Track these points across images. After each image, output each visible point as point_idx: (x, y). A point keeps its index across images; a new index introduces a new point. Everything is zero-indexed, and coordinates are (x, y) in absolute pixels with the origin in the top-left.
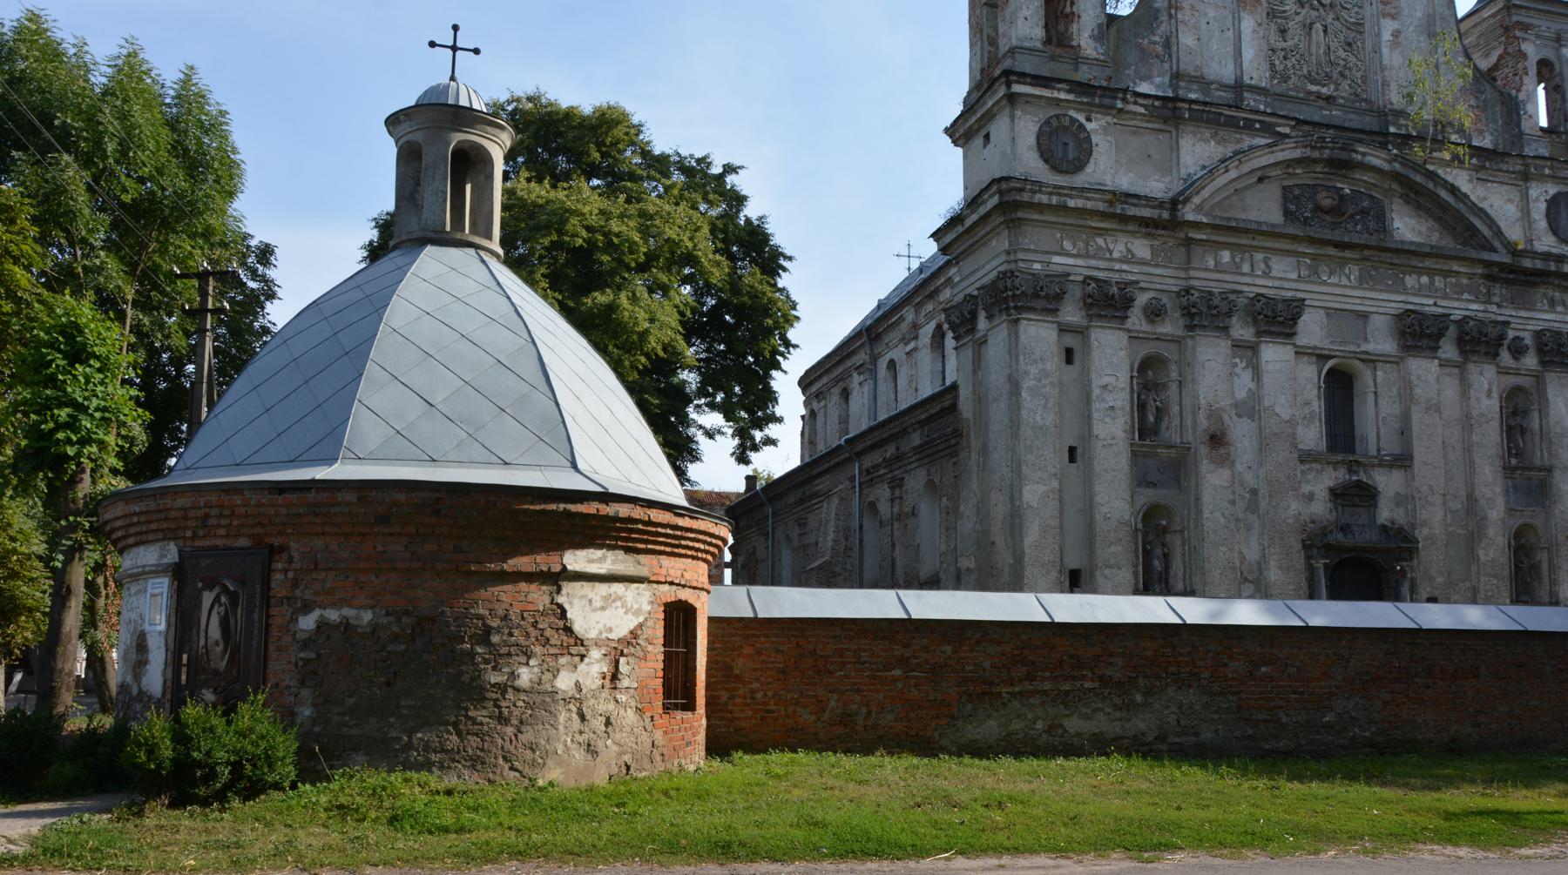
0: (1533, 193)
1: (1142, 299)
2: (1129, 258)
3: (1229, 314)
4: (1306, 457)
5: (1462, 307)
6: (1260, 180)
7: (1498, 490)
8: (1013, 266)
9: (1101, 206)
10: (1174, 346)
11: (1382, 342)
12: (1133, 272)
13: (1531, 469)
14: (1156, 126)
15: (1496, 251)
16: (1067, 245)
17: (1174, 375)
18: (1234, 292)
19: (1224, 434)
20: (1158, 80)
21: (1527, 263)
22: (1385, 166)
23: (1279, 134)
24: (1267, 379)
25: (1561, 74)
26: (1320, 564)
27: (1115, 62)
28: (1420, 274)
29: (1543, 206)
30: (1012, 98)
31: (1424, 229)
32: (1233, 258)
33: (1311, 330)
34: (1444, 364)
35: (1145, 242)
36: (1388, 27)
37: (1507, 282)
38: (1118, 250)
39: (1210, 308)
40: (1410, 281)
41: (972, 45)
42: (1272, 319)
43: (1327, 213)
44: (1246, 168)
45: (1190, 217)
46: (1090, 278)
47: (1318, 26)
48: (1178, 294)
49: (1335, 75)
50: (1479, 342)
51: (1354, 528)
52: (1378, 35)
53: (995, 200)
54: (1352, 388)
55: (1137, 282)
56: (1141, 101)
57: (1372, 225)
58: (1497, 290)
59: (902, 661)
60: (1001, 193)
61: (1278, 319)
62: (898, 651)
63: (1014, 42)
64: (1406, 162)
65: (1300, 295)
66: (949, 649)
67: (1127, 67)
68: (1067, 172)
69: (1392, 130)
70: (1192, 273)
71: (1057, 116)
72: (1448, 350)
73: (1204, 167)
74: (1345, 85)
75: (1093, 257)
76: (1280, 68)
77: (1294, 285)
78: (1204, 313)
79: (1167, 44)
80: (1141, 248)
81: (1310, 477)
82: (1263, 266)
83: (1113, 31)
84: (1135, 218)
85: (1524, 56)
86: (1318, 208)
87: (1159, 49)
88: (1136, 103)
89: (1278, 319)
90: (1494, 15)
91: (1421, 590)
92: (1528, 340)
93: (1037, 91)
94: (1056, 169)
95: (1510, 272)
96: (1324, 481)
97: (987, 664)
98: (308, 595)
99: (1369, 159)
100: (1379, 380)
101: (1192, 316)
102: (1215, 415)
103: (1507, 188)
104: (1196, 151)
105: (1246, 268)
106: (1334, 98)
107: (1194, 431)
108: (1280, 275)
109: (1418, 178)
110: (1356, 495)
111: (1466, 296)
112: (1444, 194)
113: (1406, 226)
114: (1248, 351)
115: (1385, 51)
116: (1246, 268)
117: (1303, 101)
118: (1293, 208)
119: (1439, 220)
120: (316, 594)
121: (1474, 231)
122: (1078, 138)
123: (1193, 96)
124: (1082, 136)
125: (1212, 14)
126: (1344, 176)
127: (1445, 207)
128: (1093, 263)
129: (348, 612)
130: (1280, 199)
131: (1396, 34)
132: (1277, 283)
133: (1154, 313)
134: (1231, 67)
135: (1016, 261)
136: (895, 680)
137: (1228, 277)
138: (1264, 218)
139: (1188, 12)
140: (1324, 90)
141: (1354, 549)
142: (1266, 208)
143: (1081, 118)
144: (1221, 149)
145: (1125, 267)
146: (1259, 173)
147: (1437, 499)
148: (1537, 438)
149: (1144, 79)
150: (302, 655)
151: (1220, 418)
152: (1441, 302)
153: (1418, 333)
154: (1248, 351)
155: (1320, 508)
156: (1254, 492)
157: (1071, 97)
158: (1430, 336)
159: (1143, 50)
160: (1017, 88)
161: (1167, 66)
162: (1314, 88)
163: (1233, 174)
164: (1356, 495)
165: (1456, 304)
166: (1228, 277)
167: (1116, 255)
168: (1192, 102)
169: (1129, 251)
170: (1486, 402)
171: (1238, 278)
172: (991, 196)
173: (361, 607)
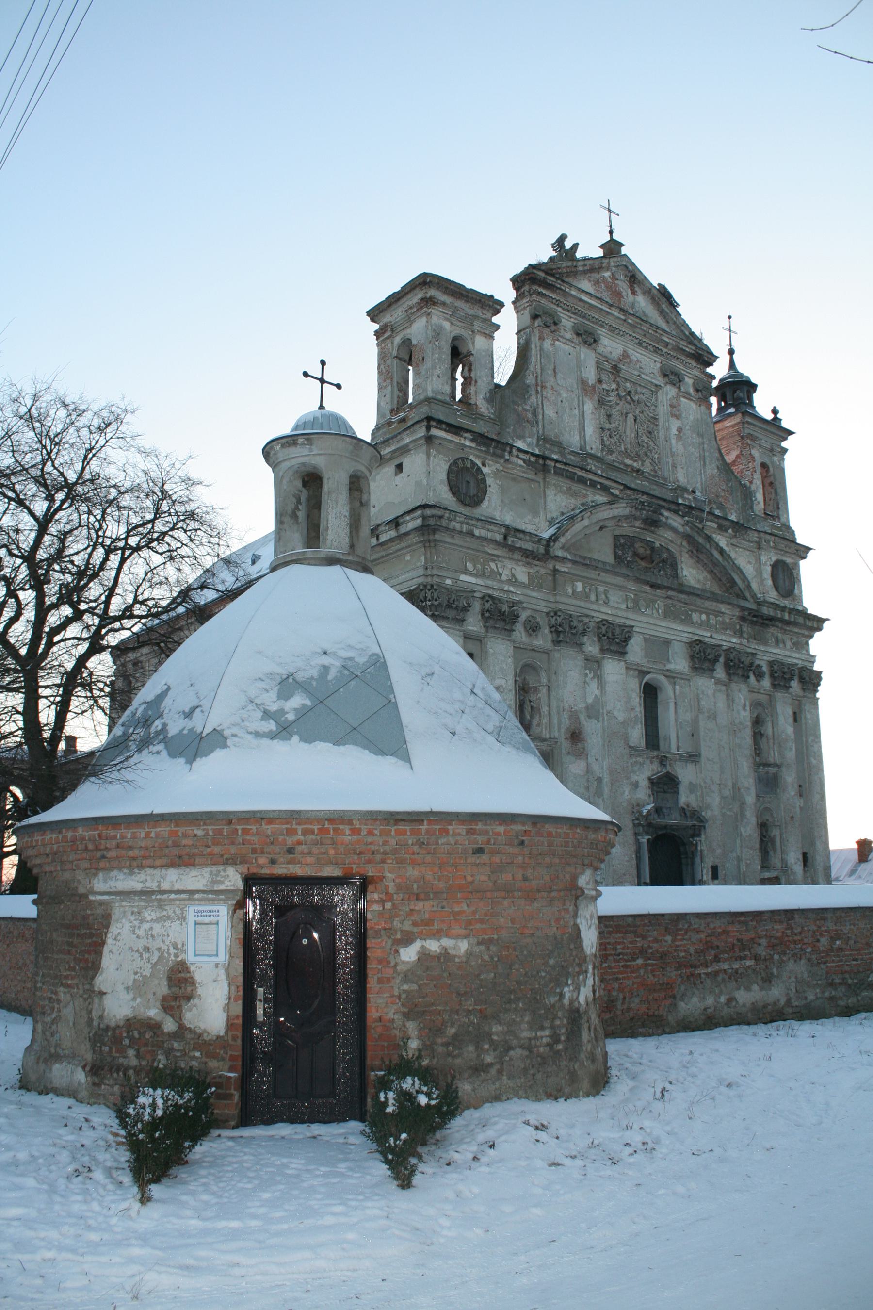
0: (763, 559)
1: (524, 616)
2: (513, 580)
3: (584, 633)
4: (634, 750)
5: (727, 640)
6: (601, 528)
7: (751, 781)
8: (429, 580)
9: (499, 537)
10: (545, 656)
11: (680, 663)
12: (517, 594)
13: (769, 765)
14: (530, 476)
15: (747, 600)
16: (470, 566)
17: (544, 680)
18: (587, 616)
19: (580, 733)
20: (529, 440)
21: (765, 610)
22: (681, 529)
23: (612, 494)
24: (609, 689)
25: (774, 475)
26: (644, 839)
27: (499, 420)
28: (701, 613)
29: (769, 569)
30: (429, 439)
31: (701, 578)
32: (584, 588)
33: (636, 649)
34: (718, 682)
35: (524, 569)
36: (675, 424)
37: (753, 623)
38: (505, 575)
39: (571, 627)
40: (695, 617)
41: (380, 389)
42: (612, 639)
43: (642, 559)
44: (594, 519)
45: (560, 553)
46: (490, 596)
47: (630, 416)
48: (548, 614)
49: (641, 453)
50: (739, 667)
51: (665, 810)
52: (668, 429)
53: (419, 522)
54: (656, 698)
55: (520, 602)
56: (521, 455)
57: (669, 571)
58: (746, 628)
59: (642, 952)
60: (424, 518)
61: (615, 639)
62: (640, 943)
63: (430, 394)
64: (693, 527)
65: (628, 623)
66: (669, 938)
67: (509, 428)
68: (469, 505)
69: (680, 501)
70: (559, 598)
71: (462, 459)
72: (720, 672)
73: (563, 514)
74: (648, 462)
75: (489, 577)
76: (607, 443)
77: (625, 614)
78: (565, 630)
79: (534, 413)
80: (522, 573)
81: (636, 768)
82: (603, 596)
83: (498, 396)
84: (520, 549)
85: (753, 458)
86: (636, 554)
87: (530, 415)
88: (517, 456)
89: (615, 639)
90: (733, 426)
91: (707, 860)
92: (765, 668)
93: (449, 436)
94: (462, 502)
95: (754, 616)
96: (645, 772)
97: (692, 950)
98: (407, 926)
99: (670, 521)
100: (677, 692)
101: (558, 633)
102: (574, 716)
103: (748, 553)
104: (557, 500)
105: (593, 597)
106: (643, 472)
107: (559, 729)
108: (613, 602)
109: (701, 540)
110: (665, 785)
111: (728, 632)
112: (716, 554)
113: (691, 573)
114: (593, 664)
115: (674, 441)
116: (593, 597)
117: (624, 471)
118: (620, 552)
119: (711, 572)
120: (415, 924)
121: (733, 583)
122: (477, 479)
123: (555, 457)
124: (480, 477)
125: (564, 395)
126: (653, 532)
127: (716, 564)
128: (489, 583)
129: (447, 942)
130: (612, 546)
131: (680, 430)
132: (614, 612)
133: (533, 628)
134: (577, 438)
135: (432, 576)
136: (639, 967)
137: (582, 604)
138: (602, 558)
139: (550, 391)
140: (635, 464)
141: (665, 827)
142: (604, 552)
143: (479, 463)
144: (573, 501)
145: (511, 589)
146: (601, 524)
147: (715, 788)
148: (771, 741)
149: (521, 437)
150: (405, 987)
151: (578, 718)
152: (715, 636)
153: (703, 657)
154: (593, 664)
155: (643, 793)
156: (599, 780)
157: (473, 445)
158: (709, 660)
159: (518, 415)
160: (435, 432)
161: (535, 430)
162: (628, 462)
163: (586, 522)
164: (665, 785)
165: (723, 638)
166: (582, 604)
167: (504, 578)
168: (557, 461)
169: (513, 576)
170: (743, 713)
171: (588, 605)
172: (413, 519)
173: (458, 937)
